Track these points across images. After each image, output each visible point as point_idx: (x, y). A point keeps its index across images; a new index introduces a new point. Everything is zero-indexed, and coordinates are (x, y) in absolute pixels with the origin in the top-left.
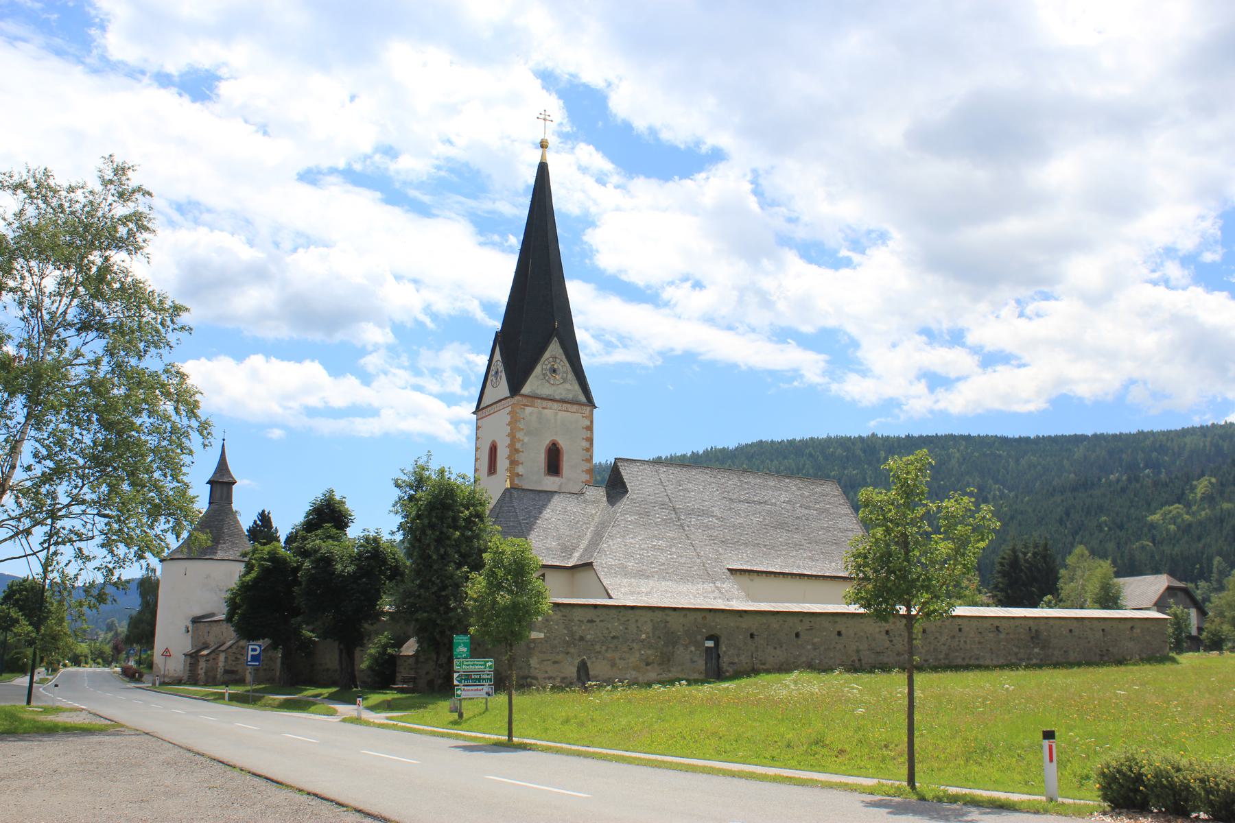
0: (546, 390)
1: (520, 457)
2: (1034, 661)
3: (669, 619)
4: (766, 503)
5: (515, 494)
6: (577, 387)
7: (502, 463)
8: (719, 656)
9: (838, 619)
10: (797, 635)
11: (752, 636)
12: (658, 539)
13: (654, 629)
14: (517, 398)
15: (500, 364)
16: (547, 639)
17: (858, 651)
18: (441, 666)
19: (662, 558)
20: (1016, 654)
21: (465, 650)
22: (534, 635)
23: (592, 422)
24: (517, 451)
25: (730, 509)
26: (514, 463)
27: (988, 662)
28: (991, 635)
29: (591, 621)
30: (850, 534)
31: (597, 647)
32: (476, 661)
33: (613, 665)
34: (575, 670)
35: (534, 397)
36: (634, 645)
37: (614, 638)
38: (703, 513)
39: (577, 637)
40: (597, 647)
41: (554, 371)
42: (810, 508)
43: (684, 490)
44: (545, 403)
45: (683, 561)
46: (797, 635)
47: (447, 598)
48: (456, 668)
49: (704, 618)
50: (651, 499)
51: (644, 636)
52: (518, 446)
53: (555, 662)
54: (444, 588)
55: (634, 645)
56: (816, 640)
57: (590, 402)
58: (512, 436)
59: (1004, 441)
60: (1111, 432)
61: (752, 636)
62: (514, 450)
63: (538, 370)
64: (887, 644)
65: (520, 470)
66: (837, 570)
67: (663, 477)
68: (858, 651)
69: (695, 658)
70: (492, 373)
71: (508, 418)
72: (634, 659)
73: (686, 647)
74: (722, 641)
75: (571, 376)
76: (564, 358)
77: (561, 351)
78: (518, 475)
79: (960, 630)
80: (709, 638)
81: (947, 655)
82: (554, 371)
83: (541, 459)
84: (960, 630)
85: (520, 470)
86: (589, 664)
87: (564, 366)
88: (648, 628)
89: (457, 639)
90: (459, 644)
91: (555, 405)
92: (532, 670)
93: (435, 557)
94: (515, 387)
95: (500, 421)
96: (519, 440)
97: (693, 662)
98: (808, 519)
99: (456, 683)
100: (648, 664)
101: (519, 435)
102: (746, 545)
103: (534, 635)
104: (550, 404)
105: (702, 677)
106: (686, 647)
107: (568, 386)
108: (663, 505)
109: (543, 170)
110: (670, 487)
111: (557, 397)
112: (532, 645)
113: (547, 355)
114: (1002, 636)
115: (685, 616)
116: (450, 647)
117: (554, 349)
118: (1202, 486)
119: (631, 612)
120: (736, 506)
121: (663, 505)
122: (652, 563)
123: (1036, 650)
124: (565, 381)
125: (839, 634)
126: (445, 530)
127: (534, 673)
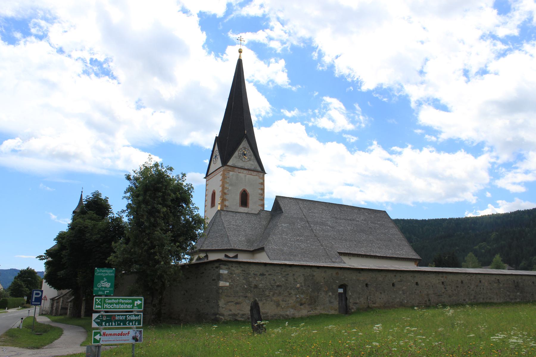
0: (240, 164)
1: (227, 197)
2: (518, 300)
3: (315, 273)
4: (353, 220)
5: (223, 213)
6: (256, 163)
7: (218, 200)
8: (346, 299)
9: (416, 275)
10: (393, 285)
11: (367, 285)
12: (300, 236)
13: (305, 280)
14: (225, 167)
15: (217, 152)
16: (231, 287)
17: (428, 295)
18: (154, 306)
19: (303, 246)
20: (509, 296)
21: (108, 285)
22: (222, 284)
23: (264, 181)
24: (225, 194)
25: (336, 223)
26: (223, 200)
27: (495, 301)
28: (496, 285)
29: (262, 275)
30: (396, 236)
31: (267, 293)
32: (121, 299)
33: (278, 305)
34: (249, 308)
35: (234, 167)
36: (292, 291)
37: (278, 286)
38: (323, 224)
39: (253, 285)
40: (267, 293)
41: (245, 155)
42: (375, 224)
43: (312, 212)
44: (240, 170)
45: (314, 247)
46: (393, 285)
47: (155, 254)
48: (96, 307)
49: (337, 273)
50: (295, 216)
51: (298, 285)
52: (226, 191)
53: (237, 303)
54: (154, 247)
55: (292, 291)
56: (404, 288)
57: (263, 171)
58: (223, 186)
59: (417, 221)
60: (455, 217)
61: (367, 285)
62: (224, 193)
63: (236, 154)
64: (443, 290)
65: (227, 203)
66: (392, 254)
67: (301, 206)
68: (428, 295)
69: (332, 300)
70: (214, 157)
71: (221, 177)
72: (292, 301)
73: (326, 292)
74: (348, 289)
75: (253, 157)
76: (249, 149)
77: (248, 145)
78: (226, 206)
79: (480, 282)
80: (340, 287)
81: (475, 296)
82: (245, 155)
83: (238, 198)
84: (480, 282)
85: (227, 203)
86: (260, 304)
87: (249, 152)
88: (301, 279)
89: (99, 272)
90: (102, 278)
91: (245, 172)
92: (220, 309)
93: (146, 224)
94: (224, 162)
95: (217, 179)
96: (226, 188)
97: (331, 302)
98: (375, 228)
99: (94, 325)
100: (301, 304)
101: (226, 186)
102: (346, 240)
103: (222, 284)
104: (242, 171)
105: (336, 313)
106: (326, 292)
107: (251, 162)
108: (301, 219)
109: (240, 63)
110: (305, 211)
111: (246, 168)
112: (220, 291)
113: (241, 146)
114: (501, 285)
115: (325, 272)
116: (90, 282)
117: (244, 144)
118: (494, 235)
119: (289, 269)
120: (339, 221)
121: (301, 219)
122: (297, 248)
123: (518, 294)
124: (250, 160)
125: (417, 284)
126: (156, 206)
127: (221, 311)
